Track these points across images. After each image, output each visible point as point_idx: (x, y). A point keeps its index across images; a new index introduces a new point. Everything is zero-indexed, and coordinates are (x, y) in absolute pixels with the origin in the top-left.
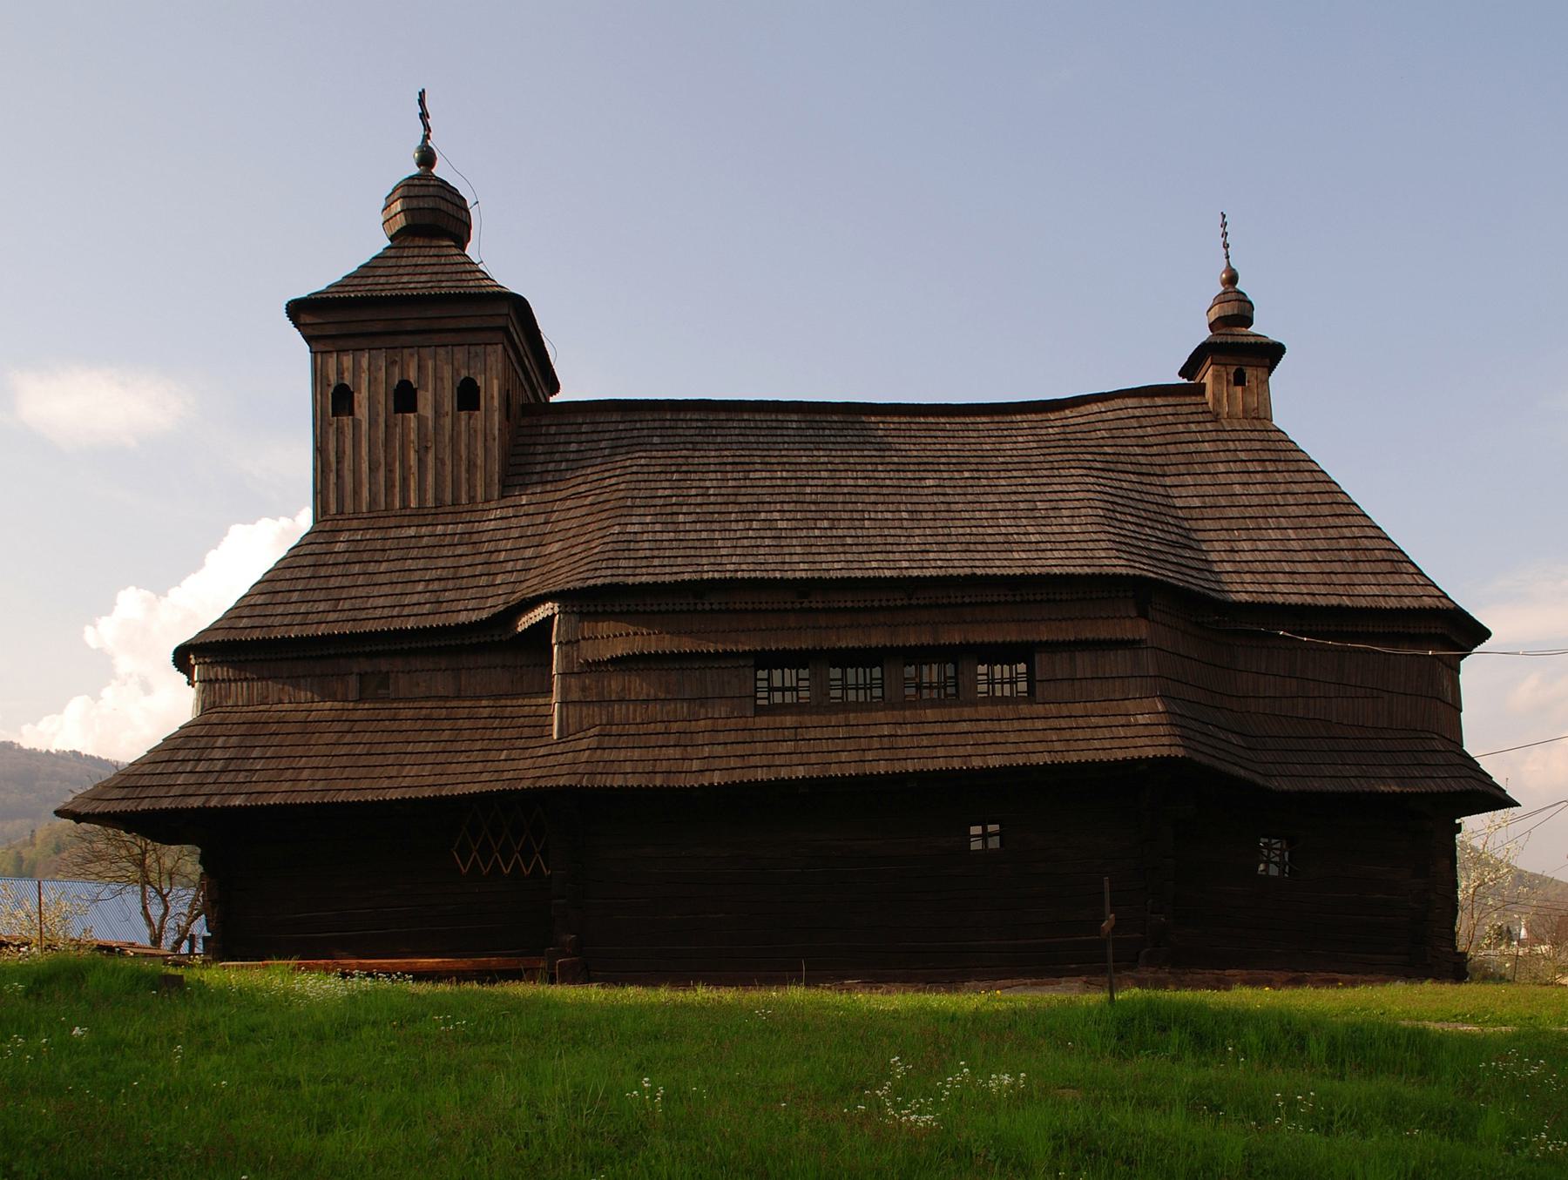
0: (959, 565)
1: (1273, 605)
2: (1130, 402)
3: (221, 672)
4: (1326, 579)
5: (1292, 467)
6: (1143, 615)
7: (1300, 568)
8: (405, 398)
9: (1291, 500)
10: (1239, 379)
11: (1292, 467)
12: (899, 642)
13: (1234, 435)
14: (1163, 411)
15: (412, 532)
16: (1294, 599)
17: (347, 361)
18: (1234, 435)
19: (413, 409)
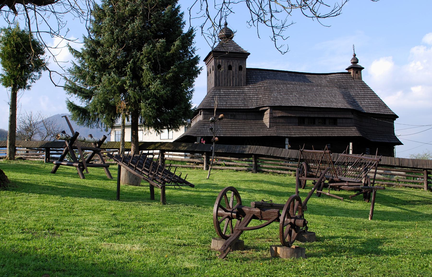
0: (324, 105)
1: (369, 113)
2: (339, 75)
3: (207, 113)
4: (376, 109)
5: (367, 89)
6: (352, 114)
7: (372, 107)
8: (230, 68)
9: (368, 95)
10: (357, 73)
11: (367, 89)
12: (319, 116)
13: (357, 82)
14: (345, 77)
15: (233, 90)
16: (372, 112)
17: (220, 61)
18: (357, 82)
19: (231, 70)
